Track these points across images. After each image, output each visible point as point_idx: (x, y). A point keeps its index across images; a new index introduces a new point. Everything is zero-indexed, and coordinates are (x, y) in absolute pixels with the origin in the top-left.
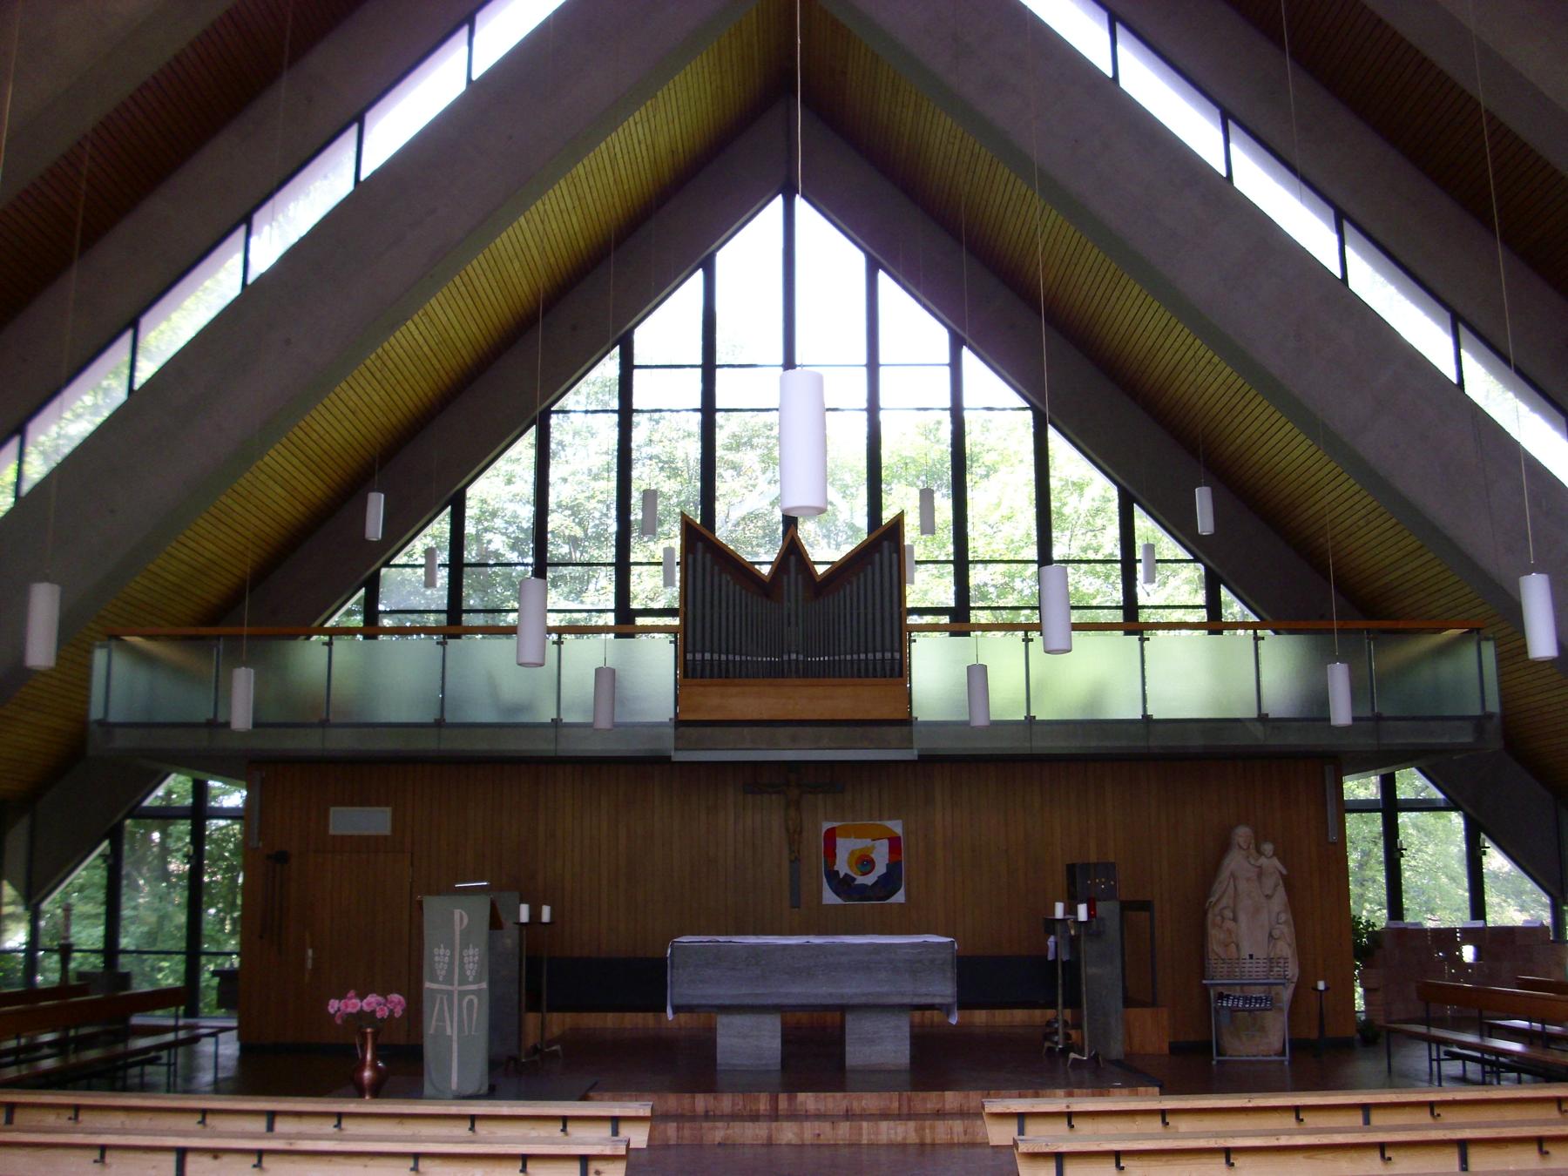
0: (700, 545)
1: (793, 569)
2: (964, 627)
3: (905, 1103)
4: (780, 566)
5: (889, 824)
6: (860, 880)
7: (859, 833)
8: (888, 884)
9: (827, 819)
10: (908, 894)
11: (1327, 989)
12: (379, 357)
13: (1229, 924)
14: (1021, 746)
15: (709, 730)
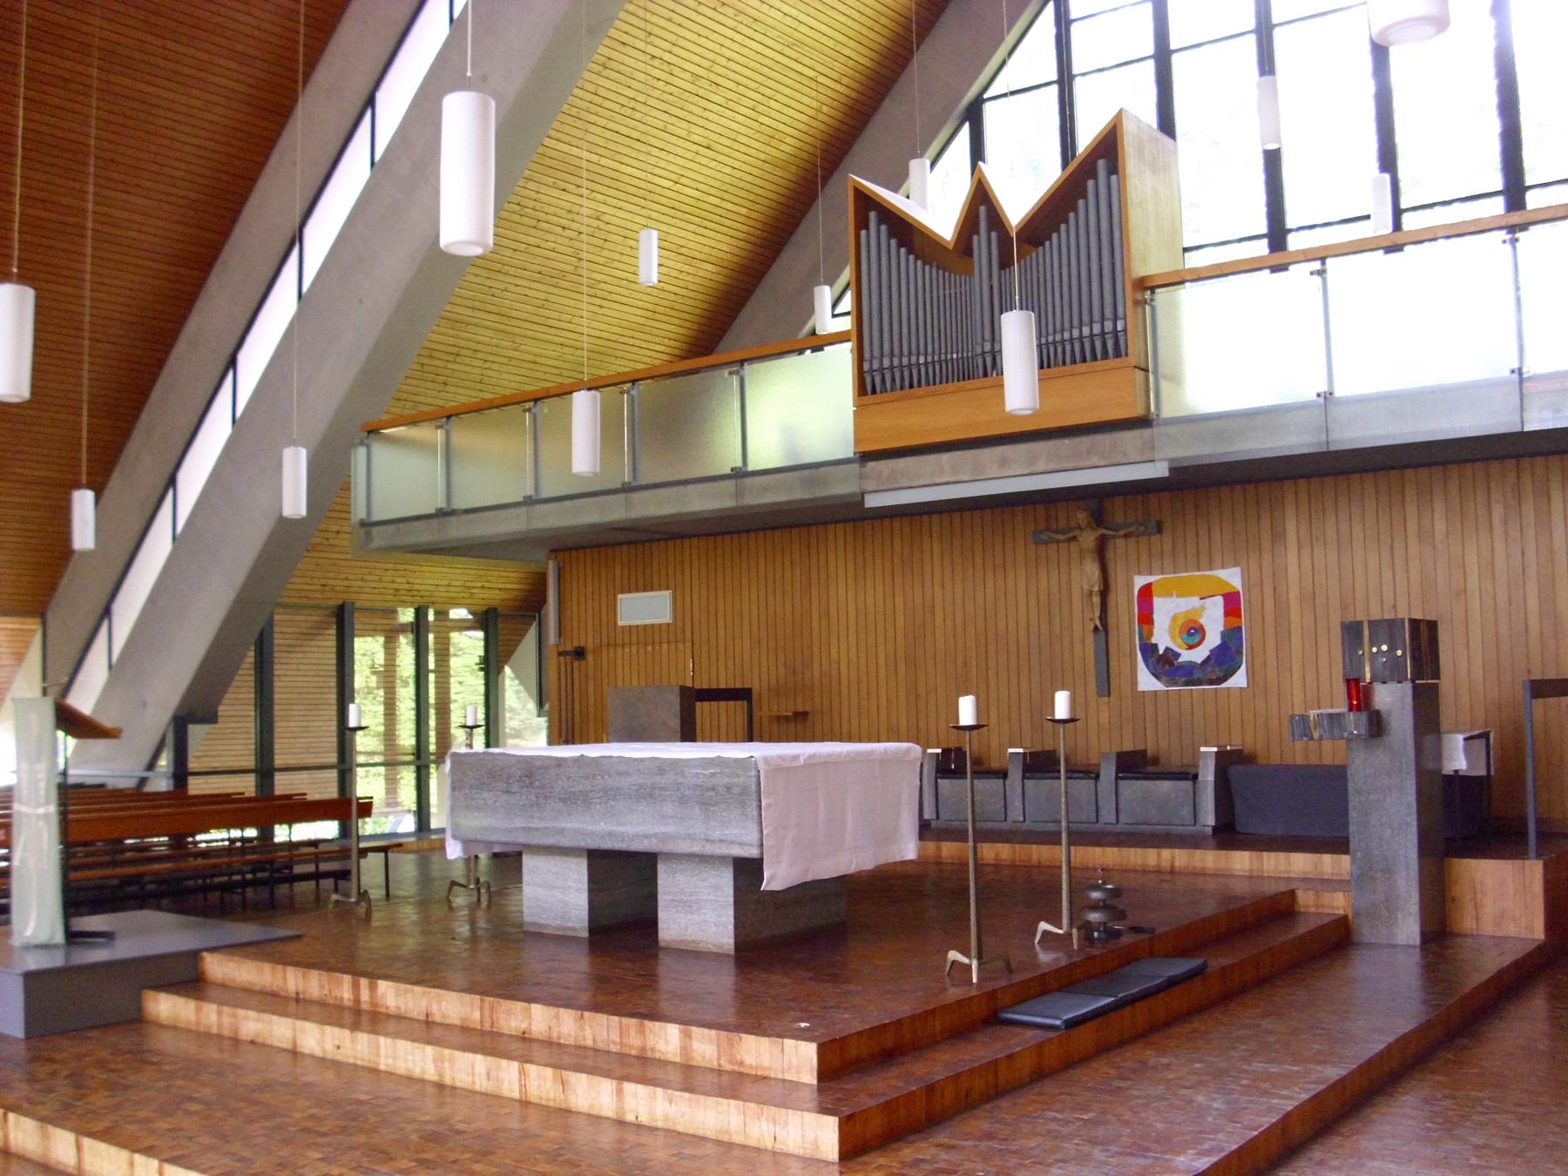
0: (873, 215)
3: (487, 1013)
4: (969, 224)
5: (1223, 574)
6: (1187, 656)
8: (1225, 658)
9: (1139, 573)
10: (1251, 675)
12: (100, 48)
15: (901, 463)
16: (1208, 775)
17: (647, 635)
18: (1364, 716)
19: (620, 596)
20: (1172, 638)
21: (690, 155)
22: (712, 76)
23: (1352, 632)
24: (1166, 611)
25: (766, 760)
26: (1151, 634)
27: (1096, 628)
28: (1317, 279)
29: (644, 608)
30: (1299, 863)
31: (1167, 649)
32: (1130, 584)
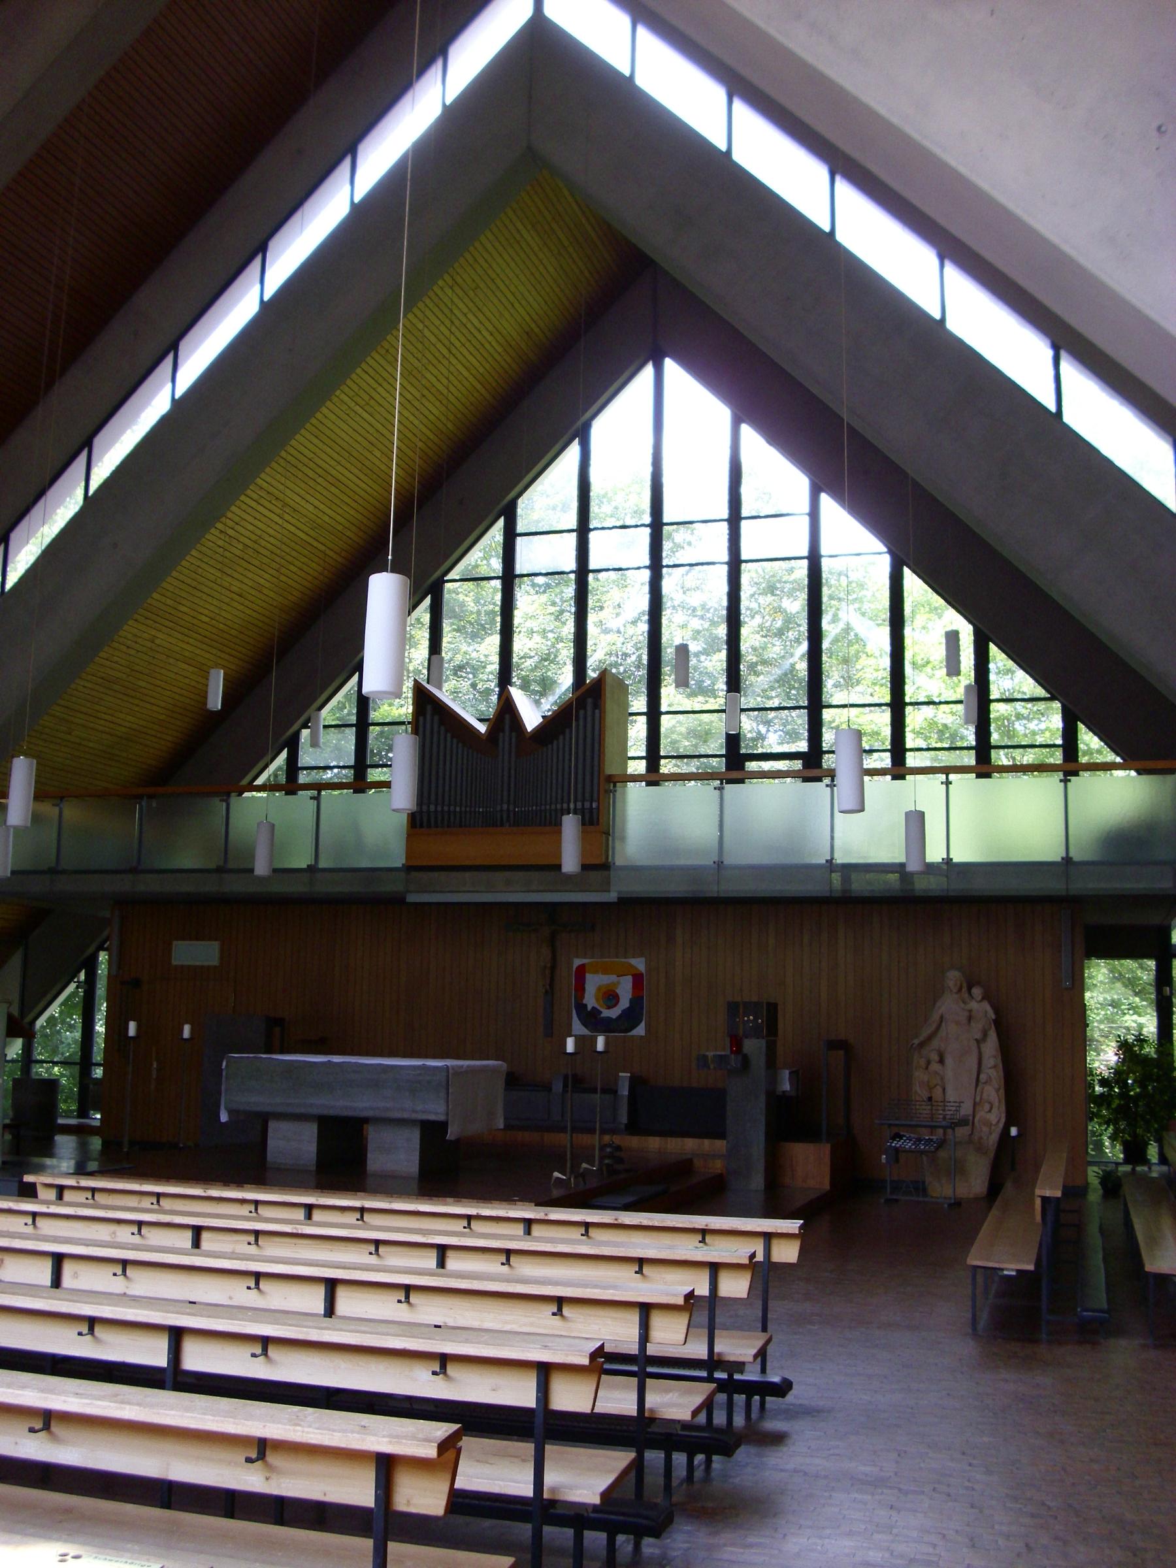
0: (429, 707)
1: (507, 727)
2: (815, 772)
5: (633, 961)
6: (606, 1013)
7: (606, 971)
8: (631, 1017)
9: (577, 957)
10: (648, 1029)
11: (1019, 1135)
13: (935, 1066)
14: (1055, 886)
16: (624, 1091)
17: (197, 973)
18: (740, 1058)
19: (175, 943)
20: (597, 1000)
21: (227, 600)
22: (256, 546)
23: (733, 1009)
24: (594, 983)
25: (453, 1067)
26: (583, 997)
27: (546, 992)
28: (717, 792)
29: (196, 953)
30: (690, 1145)
31: (593, 1008)
32: (570, 964)
